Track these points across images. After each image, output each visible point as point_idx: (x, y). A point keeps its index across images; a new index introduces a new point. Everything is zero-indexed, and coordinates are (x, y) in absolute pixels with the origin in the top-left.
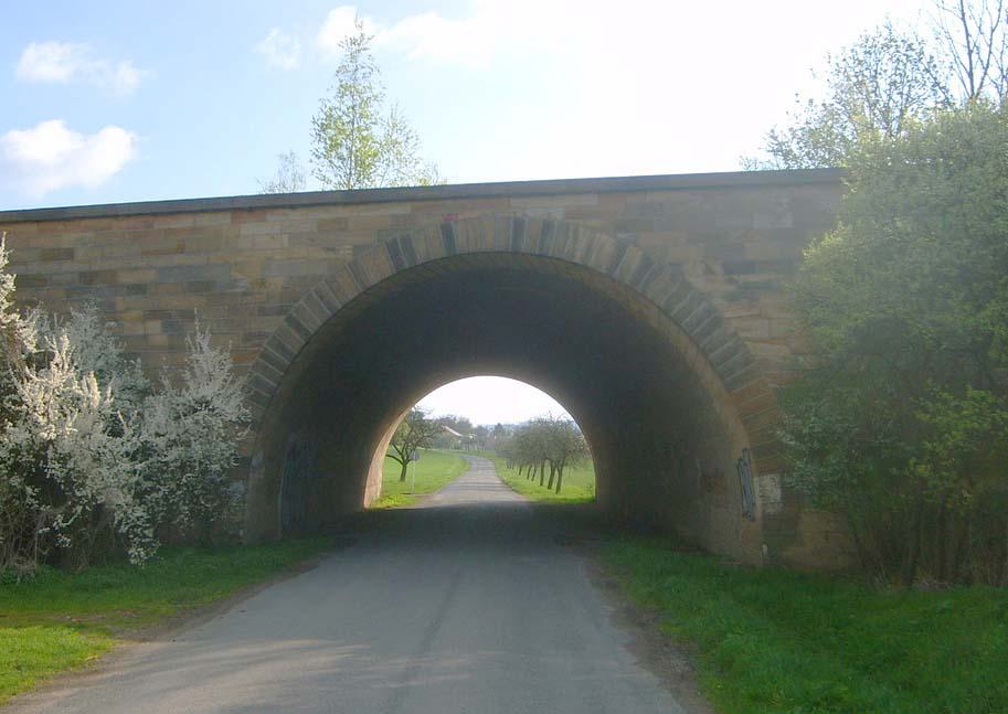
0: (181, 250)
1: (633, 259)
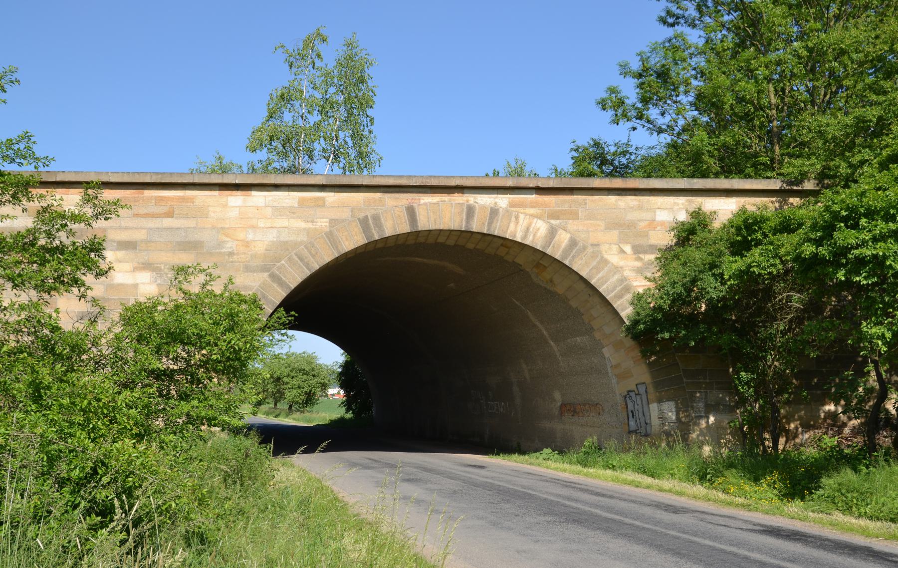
0: (170, 214)
1: (563, 238)
